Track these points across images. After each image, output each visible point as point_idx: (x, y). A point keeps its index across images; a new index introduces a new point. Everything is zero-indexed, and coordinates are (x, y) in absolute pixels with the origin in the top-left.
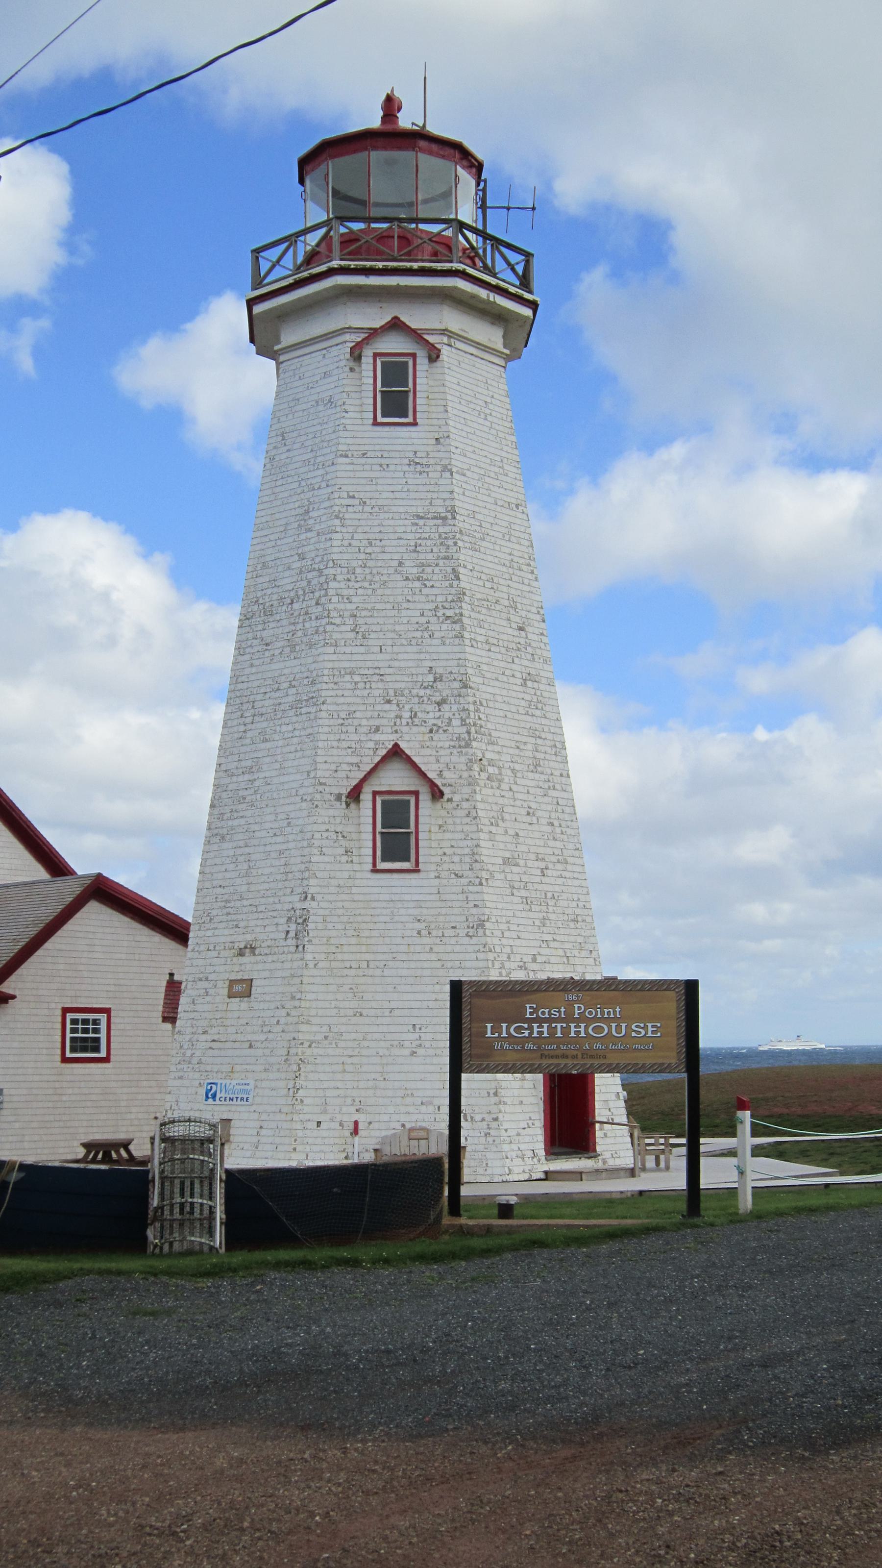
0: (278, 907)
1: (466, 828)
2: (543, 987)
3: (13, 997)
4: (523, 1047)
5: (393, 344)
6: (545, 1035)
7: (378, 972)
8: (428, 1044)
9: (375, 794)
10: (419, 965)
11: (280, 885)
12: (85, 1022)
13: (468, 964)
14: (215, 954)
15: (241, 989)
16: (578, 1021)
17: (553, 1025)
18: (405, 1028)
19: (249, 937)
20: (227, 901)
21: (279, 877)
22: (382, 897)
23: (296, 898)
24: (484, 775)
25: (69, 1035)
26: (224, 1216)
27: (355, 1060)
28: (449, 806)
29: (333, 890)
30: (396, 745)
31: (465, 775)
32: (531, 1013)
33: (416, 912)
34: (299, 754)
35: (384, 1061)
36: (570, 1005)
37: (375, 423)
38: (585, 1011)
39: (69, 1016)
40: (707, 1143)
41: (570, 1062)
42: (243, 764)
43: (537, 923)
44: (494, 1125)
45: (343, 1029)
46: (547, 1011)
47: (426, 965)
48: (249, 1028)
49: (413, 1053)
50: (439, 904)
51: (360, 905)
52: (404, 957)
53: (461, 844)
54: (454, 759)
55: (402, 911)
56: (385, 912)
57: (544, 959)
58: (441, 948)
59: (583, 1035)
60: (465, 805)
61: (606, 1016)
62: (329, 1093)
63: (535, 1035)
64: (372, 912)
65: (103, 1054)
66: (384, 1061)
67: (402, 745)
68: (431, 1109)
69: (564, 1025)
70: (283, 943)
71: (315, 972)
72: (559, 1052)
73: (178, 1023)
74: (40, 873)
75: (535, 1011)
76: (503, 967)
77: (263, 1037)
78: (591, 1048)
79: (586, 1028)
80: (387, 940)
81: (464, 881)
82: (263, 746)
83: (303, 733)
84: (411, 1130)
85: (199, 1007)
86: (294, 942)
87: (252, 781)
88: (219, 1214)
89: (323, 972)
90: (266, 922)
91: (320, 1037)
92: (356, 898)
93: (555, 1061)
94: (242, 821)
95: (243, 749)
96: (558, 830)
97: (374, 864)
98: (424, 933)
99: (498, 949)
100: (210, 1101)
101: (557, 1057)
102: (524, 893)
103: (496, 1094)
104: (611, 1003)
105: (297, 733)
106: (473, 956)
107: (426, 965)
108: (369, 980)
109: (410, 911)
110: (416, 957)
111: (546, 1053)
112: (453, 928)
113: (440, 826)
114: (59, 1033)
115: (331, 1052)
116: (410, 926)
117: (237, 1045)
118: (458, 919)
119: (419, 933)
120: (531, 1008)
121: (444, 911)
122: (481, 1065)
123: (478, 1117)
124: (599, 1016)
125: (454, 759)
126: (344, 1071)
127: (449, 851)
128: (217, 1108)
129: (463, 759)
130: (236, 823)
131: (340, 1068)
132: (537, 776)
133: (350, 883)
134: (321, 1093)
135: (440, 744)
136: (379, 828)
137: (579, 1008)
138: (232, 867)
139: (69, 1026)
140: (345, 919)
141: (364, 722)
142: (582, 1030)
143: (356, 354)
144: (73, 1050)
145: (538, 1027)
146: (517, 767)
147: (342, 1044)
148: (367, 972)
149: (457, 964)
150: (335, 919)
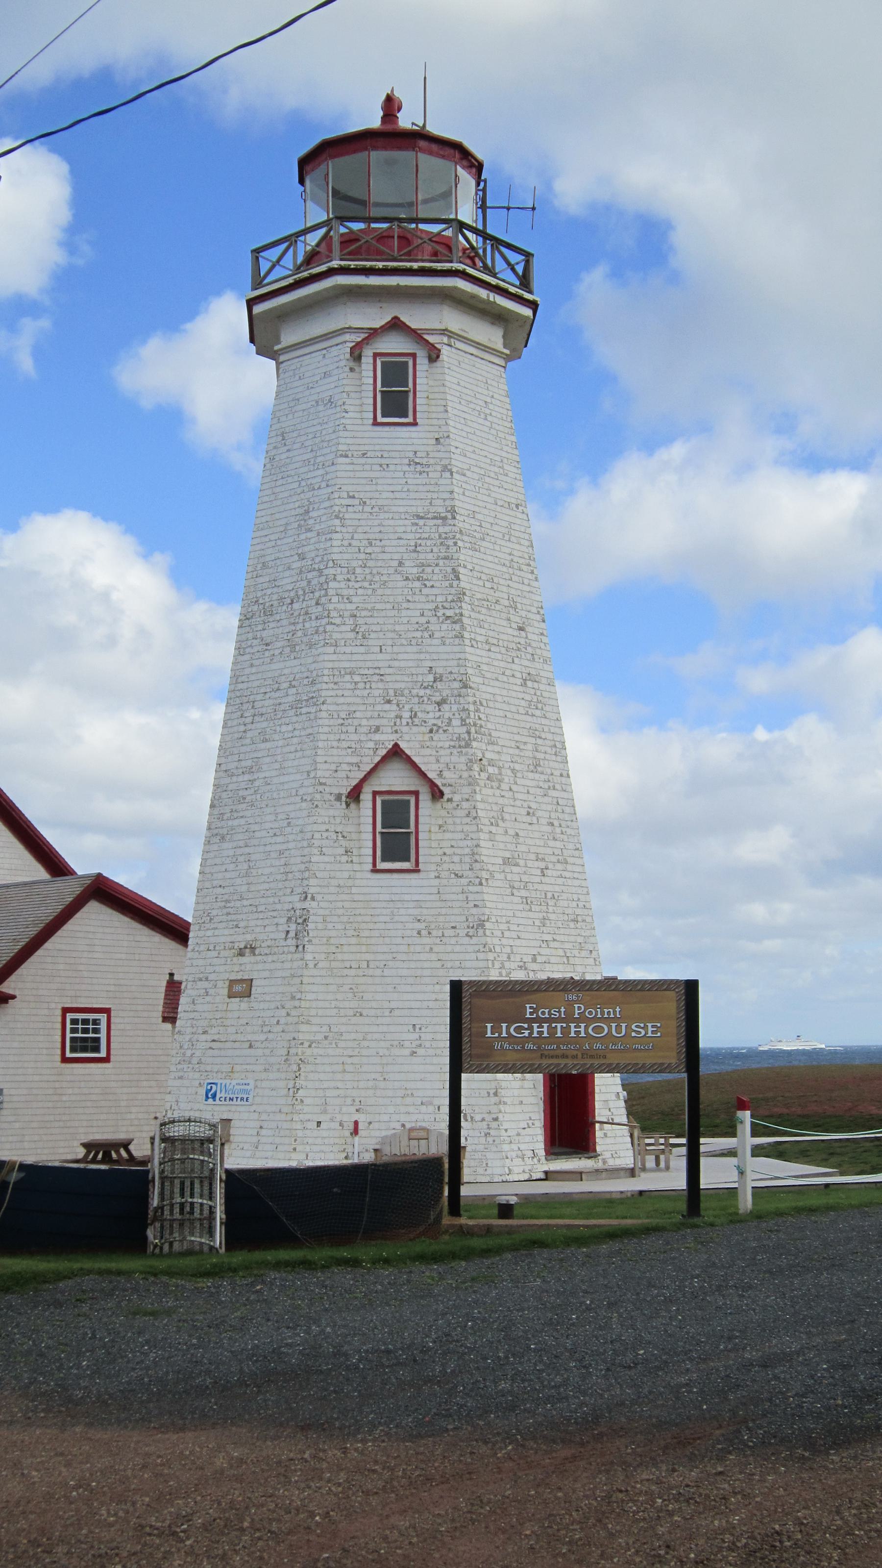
0: (278, 907)
1: (466, 828)
2: (543, 987)
3: (13, 997)
4: (523, 1047)
5: (393, 344)
6: (545, 1035)
7: (378, 972)
8: (428, 1044)
9: (375, 794)
10: (419, 965)
11: (280, 885)
12: (85, 1022)
13: (468, 964)
14: (215, 954)
15: (241, 989)
16: (578, 1021)
17: (553, 1025)
18: (405, 1028)
19: (249, 937)
20: (227, 901)
21: (279, 877)
22: (382, 897)
23: (296, 898)
24: (484, 775)
25: (69, 1035)
26: (224, 1216)
27: (355, 1060)
28: (449, 806)
29: (333, 890)
30: (396, 745)
31: (465, 775)
32: (531, 1013)
33: (416, 912)
34: (299, 754)
35: (384, 1061)
36: (570, 1005)
37: (375, 423)
38: (585, 1011)
39: (69, 1016)
40: (707, 1143)
41: (570, 1062)
42: (243, 764)
43: (537, 923)
44: (494, 1125)
45: (343, 1029)
46: (547, 1011)
47: (426, 965)
48: (249, 1028)
49: (413, 1053)
50: (439, 904)
51: (360, 905)
52: (404, 957)
53: (461, 844)
54: (454, 759)
55: (402, 911)
56: (385, 912)
57: (544, 959)
58: (441, 948)
59: (583, 1035)
60: (465, 805)
61: (606, 1016)
62: (329, 1093)
63: (535, 1035)
64: (372, 912)
65: (103, 1054)
66: (384, 1061)
67: (402, 745)
68: (431, 1109)
69: (564, 1025)
70: (283, 943)
71: (315, 972)
72: (559, 1052)
73: (178, 1023)
74: (40, 873)
75: (535, 1011)
76: (503, 967)
77: (263, 1037)
78: (591, 1048)
79: (586, 1028)
80: (387, 940)
81: (464, 881)
82: (263, 746)
83: (303, 733)
84: (411, 1130)
85: (199, 1007)
86: (294, 942)
87: (252, 781)
88: (219, 1214)
89: (323, 972)
90: (266, 922)
91: (320, 1037)
92: (356, 898)
93: (555, 1061)
94: (242, 821)
95: (243, 749)
96: (558, 830)
97: (374, 864)
98: (424, 933)
99: (498, 949)
100: (210, 1101)
101: (557, 1057)
102: (524, 893)
103: (496, 1094)
104: (611, 1003)
105: (297, 733)
106: (473, 956)
107: (426, 965)
108: (369, 980)
109: (410, 911)
110: (416, 957)
111: (546, 1053)
112: (453, 928)
113: (440, 826)
114: (59, 1033)
115: (331, 1052)
116: (410, 926)
117: (237, 1045)
118: (458, 919)
119: (419, 933)
120: (531, 1008)
121: (444, 911)
122: (481, 1065)
123: (478, 1117)
124: (599, 1016)
125: (454, 759)
126: (344, 1071)
127: (449, 851)
128: (217, 1108)
129: (463, 759)
130: (236, 823)
131: (340, 1068)
132: (537, 776)
133: (350, 883)
134: (321, 1093)
135: (440, 744)
136: (379, 828)
137: (579, 1008)
138: (232, 867)
139: (69, 1026)
140: (345, 919)
141: (364, 722)
142: (582, 1030)
143: (356, 354)
144: (73, 1050)
145: (538, 1027)
146: (517, 767)
147: (342, 1044)
148: (367, 972)
149: (457, 964)
150: (335, 919)
